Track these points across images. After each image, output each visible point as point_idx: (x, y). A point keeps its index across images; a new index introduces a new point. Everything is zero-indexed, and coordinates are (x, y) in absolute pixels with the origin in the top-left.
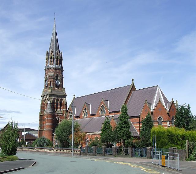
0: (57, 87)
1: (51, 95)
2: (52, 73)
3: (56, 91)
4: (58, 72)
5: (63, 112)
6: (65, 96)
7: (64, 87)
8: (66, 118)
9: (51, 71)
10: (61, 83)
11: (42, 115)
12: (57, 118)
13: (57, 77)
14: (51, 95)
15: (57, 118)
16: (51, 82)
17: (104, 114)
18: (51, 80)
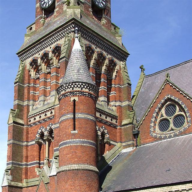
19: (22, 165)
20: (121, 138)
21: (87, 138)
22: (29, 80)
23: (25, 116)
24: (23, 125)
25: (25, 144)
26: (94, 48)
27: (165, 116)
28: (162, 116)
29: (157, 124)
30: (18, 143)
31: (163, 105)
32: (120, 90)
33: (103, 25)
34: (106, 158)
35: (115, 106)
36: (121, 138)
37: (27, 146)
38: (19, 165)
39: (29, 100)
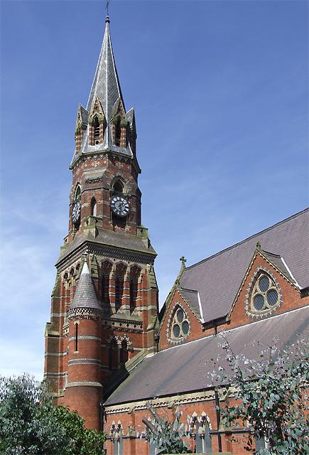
0: (119, 220)
1: (92, 246)
2: (96, 170)
3: (114, 235)
4: (122, 170)
5: (141, 319)
6: (150, 258)
7: (144, 224)
8: (157, 340)
9: (96, 164)
10: (134, 210)
11: (56, 333)
12: (119, 342)
13: (118, 187)
14: (92, 246)
15: (119, 342)
16: (93, 201)
17: (271, 308)
18: (94, 194)
19: (57, 375)
20: (146, 343)
21: (87, 357)
22: (64, 292)
23: (60, 329)
24: (59, 336)
25: (60, 354)
26: (113, 261)
27: (260, 292)
28: (256, 291)
29: (252, 301)
30: (53, 354)
31: (256, 278)
32: (145, 294)
33: (127, 232)
34: (126, 367)
35: (141, 311)
36: (146, 343)
37: (62, 356)
38: (55, 375)
39: (63, 312)
